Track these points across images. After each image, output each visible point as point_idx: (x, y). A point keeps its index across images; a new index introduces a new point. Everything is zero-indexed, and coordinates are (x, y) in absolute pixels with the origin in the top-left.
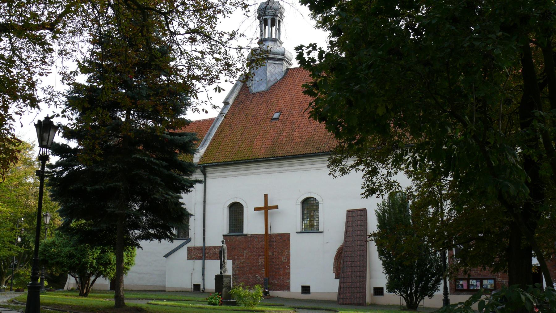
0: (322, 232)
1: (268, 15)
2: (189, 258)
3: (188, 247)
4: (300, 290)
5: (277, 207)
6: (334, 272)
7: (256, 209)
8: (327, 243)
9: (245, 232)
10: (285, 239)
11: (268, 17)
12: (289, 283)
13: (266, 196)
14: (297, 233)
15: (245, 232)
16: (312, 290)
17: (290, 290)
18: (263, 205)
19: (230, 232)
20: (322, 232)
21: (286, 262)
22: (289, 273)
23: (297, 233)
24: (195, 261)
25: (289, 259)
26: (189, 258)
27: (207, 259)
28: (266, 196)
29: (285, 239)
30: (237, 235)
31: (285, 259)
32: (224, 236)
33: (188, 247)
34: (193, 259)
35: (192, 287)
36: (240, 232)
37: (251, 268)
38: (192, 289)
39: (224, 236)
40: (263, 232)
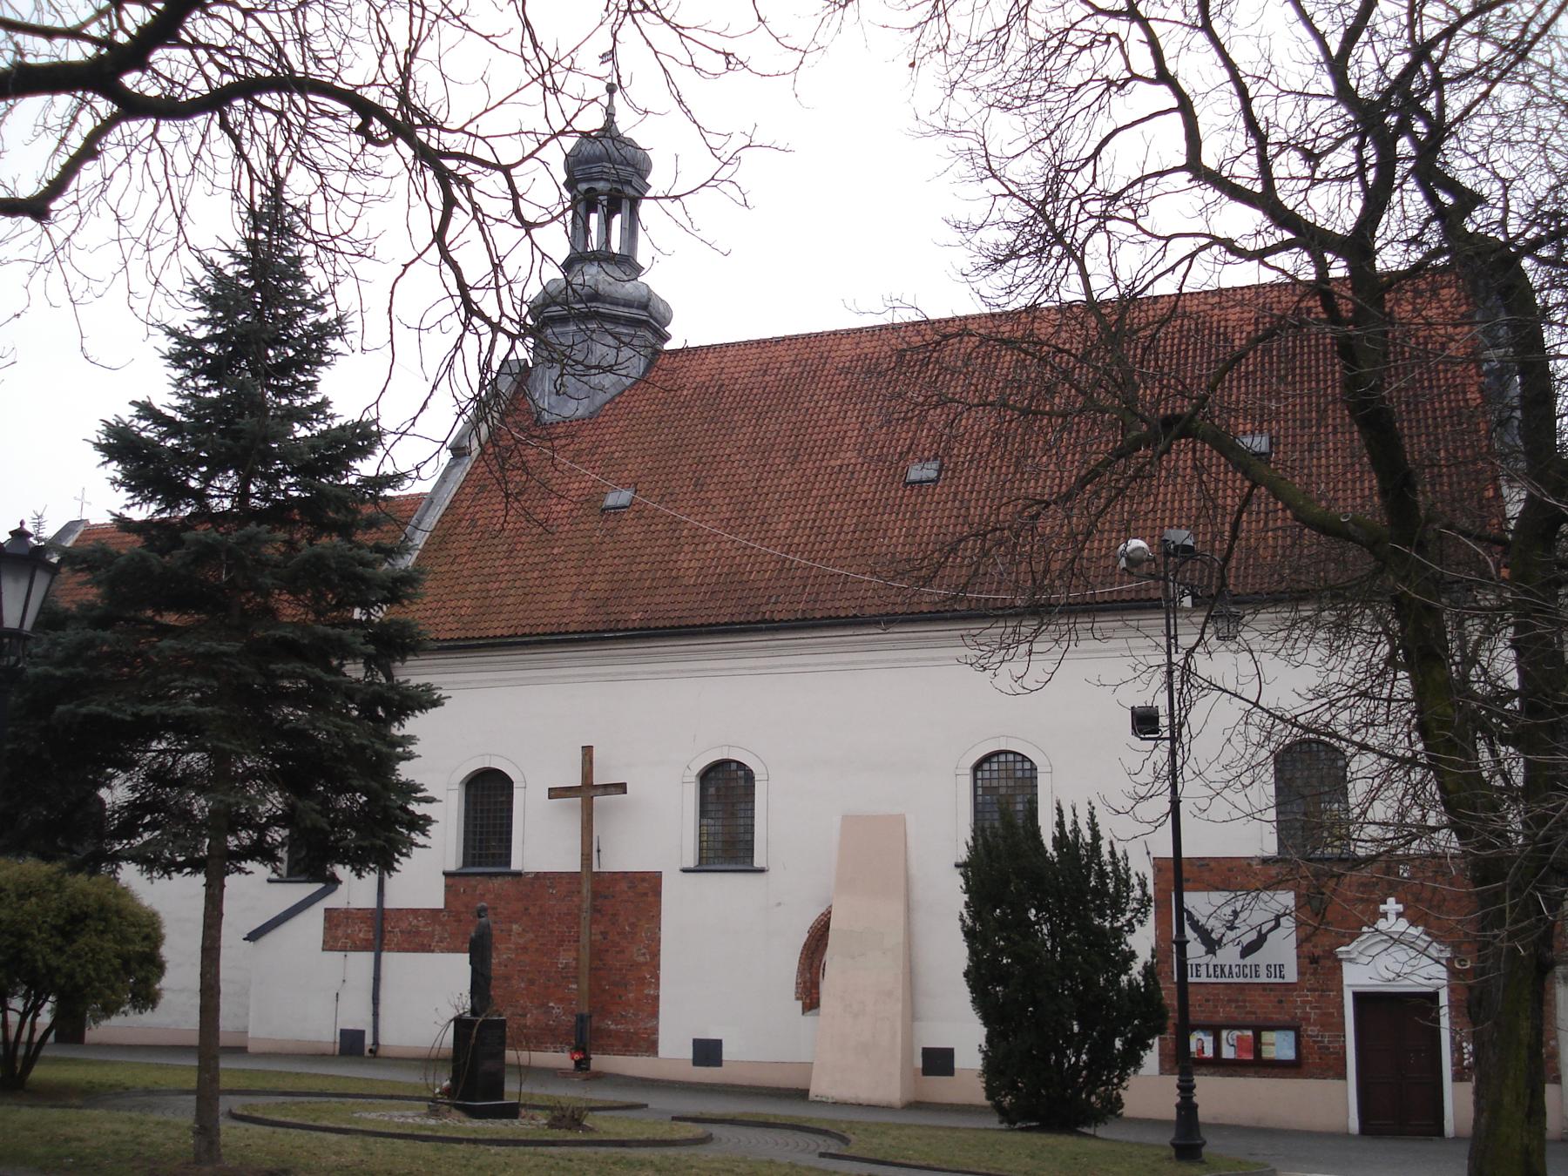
0: (762, 871)
1: (602, 179)
2: (329, 946)
3: (326, 910)
4: (688, 1054)
5: (621, 788)
6: (797, 999)
7: (555, 793)
8: (779, 904)
9: (516, 865)
10: (647, 887)
11: (600, 185)
12: (655, 1030)
13: (587, 751)
14: (685, 871)
15: (516, 865)
16: (727, 1053)
17: (655, 1053)
18: (576, 781)
19: (465, 864)
20: (762, 871)
21: (646, 963)
22: (656, 998)
23: (685, 871)
24: (349, 954)
25: (655, 954)
26: (329, 946)
27: (390, 950)
28: (587, 751)
29: (647, 887)
30: (490, 875)
31: (644, 954)
32: (447, 874)
33: (326, 910)
34: (344, 949)
35: (338, 1040)
36: (500, 865)
37: (531, 982)
38: (338, 1046)
39: (447, 874)
40: (573, 864)
